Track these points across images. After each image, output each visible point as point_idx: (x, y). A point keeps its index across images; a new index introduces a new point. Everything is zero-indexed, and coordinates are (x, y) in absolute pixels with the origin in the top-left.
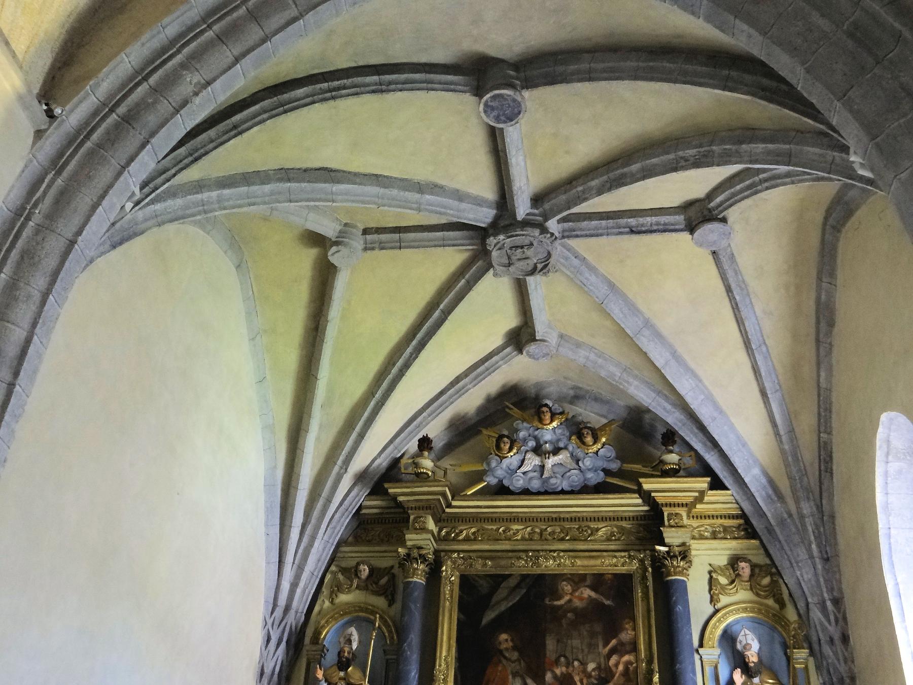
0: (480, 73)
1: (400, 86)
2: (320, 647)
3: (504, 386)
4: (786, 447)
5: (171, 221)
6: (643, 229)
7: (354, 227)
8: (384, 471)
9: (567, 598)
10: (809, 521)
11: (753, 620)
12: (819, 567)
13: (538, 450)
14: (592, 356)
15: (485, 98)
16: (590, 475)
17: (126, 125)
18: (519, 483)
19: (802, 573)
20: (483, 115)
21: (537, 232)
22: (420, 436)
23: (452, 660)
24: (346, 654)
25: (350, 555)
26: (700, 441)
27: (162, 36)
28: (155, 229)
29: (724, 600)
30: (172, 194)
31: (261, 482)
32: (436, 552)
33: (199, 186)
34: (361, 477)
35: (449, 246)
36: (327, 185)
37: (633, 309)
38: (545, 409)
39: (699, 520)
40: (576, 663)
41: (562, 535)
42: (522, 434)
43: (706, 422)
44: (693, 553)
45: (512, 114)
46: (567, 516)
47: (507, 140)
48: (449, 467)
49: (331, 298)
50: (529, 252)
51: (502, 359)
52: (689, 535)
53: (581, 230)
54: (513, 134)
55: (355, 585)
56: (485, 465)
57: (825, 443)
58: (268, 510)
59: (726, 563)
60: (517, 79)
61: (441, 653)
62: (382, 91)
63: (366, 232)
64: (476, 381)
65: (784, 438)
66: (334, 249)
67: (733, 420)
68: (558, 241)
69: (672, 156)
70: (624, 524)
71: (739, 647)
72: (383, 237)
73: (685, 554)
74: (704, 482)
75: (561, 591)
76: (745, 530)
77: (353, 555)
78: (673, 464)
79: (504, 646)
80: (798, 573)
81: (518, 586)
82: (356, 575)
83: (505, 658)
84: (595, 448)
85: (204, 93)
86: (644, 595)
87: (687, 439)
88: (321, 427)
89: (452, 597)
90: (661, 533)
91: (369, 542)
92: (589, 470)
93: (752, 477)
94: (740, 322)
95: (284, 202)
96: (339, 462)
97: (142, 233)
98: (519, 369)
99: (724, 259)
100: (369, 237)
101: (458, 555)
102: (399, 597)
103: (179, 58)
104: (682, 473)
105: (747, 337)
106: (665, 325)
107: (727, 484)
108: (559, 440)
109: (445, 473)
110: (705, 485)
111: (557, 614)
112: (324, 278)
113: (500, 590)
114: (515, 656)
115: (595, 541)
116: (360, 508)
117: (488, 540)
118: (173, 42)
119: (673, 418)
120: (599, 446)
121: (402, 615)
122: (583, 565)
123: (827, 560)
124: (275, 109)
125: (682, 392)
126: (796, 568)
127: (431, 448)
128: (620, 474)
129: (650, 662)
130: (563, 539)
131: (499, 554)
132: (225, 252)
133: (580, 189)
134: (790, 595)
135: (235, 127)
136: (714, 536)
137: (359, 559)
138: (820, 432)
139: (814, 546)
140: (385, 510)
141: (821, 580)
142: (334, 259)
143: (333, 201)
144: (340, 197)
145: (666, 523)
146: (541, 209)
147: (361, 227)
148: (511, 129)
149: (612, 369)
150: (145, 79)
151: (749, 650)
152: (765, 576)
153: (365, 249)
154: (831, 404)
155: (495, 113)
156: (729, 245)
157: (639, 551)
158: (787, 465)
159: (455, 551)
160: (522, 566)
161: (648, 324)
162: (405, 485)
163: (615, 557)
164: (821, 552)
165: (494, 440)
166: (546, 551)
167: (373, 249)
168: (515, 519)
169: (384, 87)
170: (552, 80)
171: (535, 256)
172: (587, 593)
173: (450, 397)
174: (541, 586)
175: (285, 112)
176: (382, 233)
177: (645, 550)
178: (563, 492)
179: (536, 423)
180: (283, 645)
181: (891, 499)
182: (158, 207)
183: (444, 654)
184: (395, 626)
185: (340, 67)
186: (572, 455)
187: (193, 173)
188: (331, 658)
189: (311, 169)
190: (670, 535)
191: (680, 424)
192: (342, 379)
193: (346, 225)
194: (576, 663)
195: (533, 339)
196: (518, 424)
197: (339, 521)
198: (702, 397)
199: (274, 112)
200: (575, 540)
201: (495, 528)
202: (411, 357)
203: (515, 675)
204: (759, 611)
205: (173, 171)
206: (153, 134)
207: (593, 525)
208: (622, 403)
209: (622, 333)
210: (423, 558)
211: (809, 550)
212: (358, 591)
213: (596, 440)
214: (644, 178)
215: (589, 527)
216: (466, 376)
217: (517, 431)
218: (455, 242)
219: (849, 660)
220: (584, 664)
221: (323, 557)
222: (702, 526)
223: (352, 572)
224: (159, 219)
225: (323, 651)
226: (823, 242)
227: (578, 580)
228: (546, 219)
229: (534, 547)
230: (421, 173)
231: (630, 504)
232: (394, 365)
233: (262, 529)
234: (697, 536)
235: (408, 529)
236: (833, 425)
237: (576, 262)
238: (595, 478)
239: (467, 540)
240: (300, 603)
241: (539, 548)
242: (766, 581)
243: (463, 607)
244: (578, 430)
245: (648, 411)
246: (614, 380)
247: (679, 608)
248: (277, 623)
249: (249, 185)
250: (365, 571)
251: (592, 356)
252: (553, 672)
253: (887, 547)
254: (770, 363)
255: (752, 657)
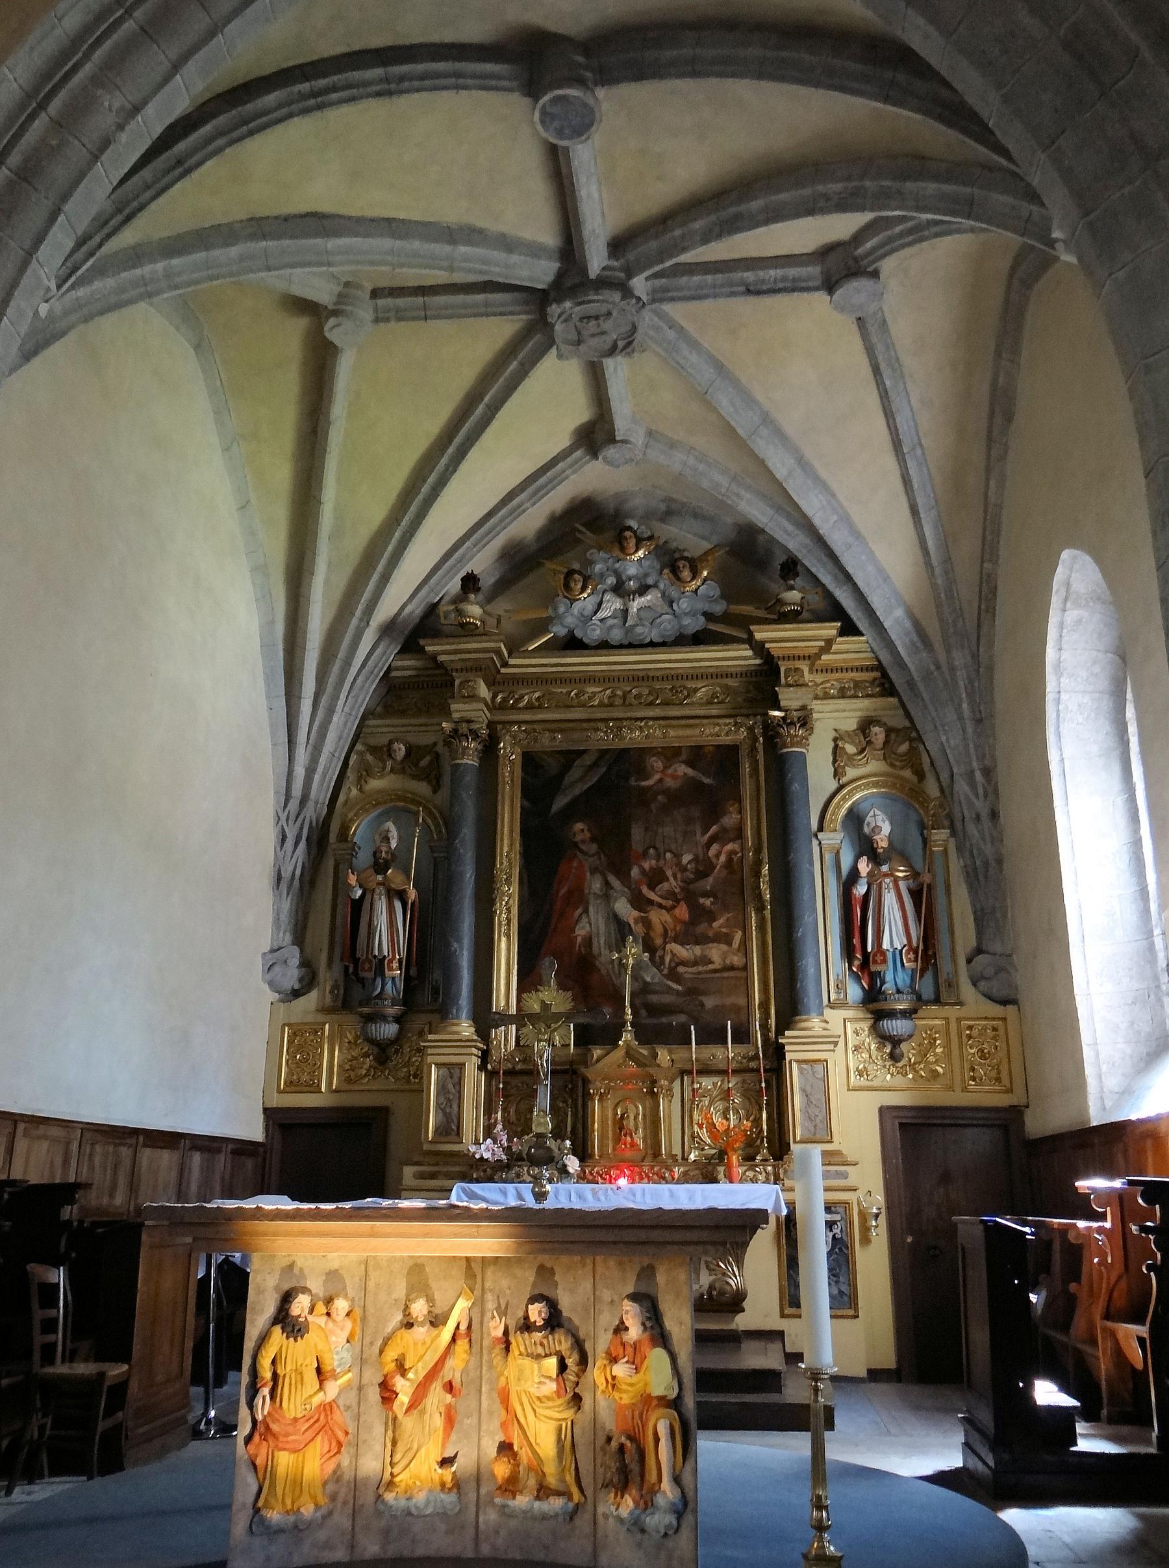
0: (534, 61)
1: (416, 84)
2: (350, 845)
3: (573, 499)
4: (939, 582)
5: (102, 312)
6: (764, 288)
7: (359, 287)
8: (417, 620)
9: (657, 777)
10: (961, 675)
11: (883, 796)
12: (970, 730)
13: (619, 589)
14: (691, 461)
15: (542, 102)
16: (687, 621)
17: (25, 185)
18: (594, 634)
19: (947, 738)
20: (539, 127)
21: (616, 296)
22: (463, 573)
23: (516, 857)
24: (383, 855)
25: (380, 730)
26: (829, 573)
27: (58, 32)
28: (82, 327)
29: (851, 773)
30: (100, 271)
31: (257, 643)
32: (491, 725)
33: (137, 256)
34: (388, 629)
35: (495, 314)
36: (318, 241)
37: (749, 400)
38: (628, 534)
39: (824, 674)
40: (668, 855)
41: (651, 698)
42: (598, 568)
43: (838, 549)
44: (815, 716)
45: (582, 126)
46: (658, 674)
47: (575, 163)
48: (501, 613)
49: (331, 390)
50: (607, 325)
51: (571, 466)
52: (811, 696)
53: (680, 289)
54: (584, 156)
55: (389, 768)
56: (550, 610)
57: (989, 575)
58: (269, 677)
59: (855, 727)
60: (586, 68)
61: (502, 850)
62: (390, 93)
63: (375, 293)
64: (533, 500)
65: (938, 571)
66: (332, 321)
67: (874, 547)
68: (648, 307)
69: (807, 192)
70: (732, 682)
71: (866, 830)
72: (401, 302)
73: (805, 720)
74: (832, 628)
75: (649, 767)
76: (882, 685)
77: (385, 730)
78: (794, 604)
79: (578, 838)
80: (944, 738)
81: (595, 764)
82: (390, 755)
83: (582, 851)
84: (693, 585)
85: (132, 126)
86: (750, 771)
87: (813, 570)
88: (329, 565)
89: (512, 781)
90: (776, 694)
91: (402, 713)
92: (686, 614)
93: (894, 619)
94: (889, 415)
95: (260, 270)
96: (358, 613)
97: (64, 333)
98: (592, 477)
99: (872, 329)
100: (381, 302)
101: (519, 727)
102: (446, 779)
103: (88, 68)
104: (805, 615)
105: (898, 435)
106: (791, 421)
107: (861, 628)
108: (646, 575)
109: (499, 621)
110: (834, 632)
111: (644, 798)
112: (320, 362)
113: (573, 769)
114: (594, 847)
115: (693, 704)
116: (389, 669)
117: (557, 706)
118: (76, 41)
119: (795, 542)
120: (699, 582)
121: (452, 805)
122: (676, 736)
123: (980, 721)
124: (235, 129)
125: (809, 512)
126: (941, 733)
127: (479, 589)
128: (726, 618)
129: (758, 850)
130: (651, 704)
131: (571, 725)
132: (177, 329)
133: (678, 232)
134: (932, 763)
135: (179, 162)
136: (842, 694)
137: (390, 736)
138: (983, 562)
139: (965, 706)
140: (423, 667)
141: (971, 746)
142: (333, 336)
143: (329, 264)
144: (338, 258)
145: (783, 681)
146: (622, 261)
147: (369, 286)
148: (580, 146)
149: (718, 477)
150: (42, 106)
151: (879, 833)
152: (900, 742)
153: (377, 320)
154: (1000, 523)
155: (556, 124)
156: (881, 308)
157: (747, 716)
158: (939, 605)
159: (513, 723)
160: (601, 739)
161: (767, 419)
162: (446, 640)
163: (718, 724)
164: (973, 712)
165: (562, 577)
166: (631, 719)
167: (388, 320)
168: (591, 679)
169: (393, 86)
170: (640, 73)
171: (613, 330)
172: (682, 769)
173: (501, 521)
174: (625, 763)
175: (251, 133)
176: (398, 296)
177: (755, 715)
178: (652, 644)
179: (617, 552)
180: (303, 844)
181: (1065, 655)
182: (81, 292)
183: (506, 849)
184: (443, 818)
185: (326, 55)
186: (663, 594)
187: (128, 237)
188: (364, 858)
189: (295, 216)
190: (787, 697)
191: (804, 551)
192: (354, 502)
193: (347, 284)
194: (668, 855)
195: (611, 440)
196: (593, 554)
197: (361, 688)
198: (835, 518)
199: (235, 135)
200: (667, 704)
201: (564, 691)
202: (447, 469)
203: (594, 871)
204: (894, 786)
205: (97, 239)
206: (65, 197)
207: (691, 684)
208: (729, 520)
209: (730, 432)
210: (475, 735)
211: (958, 710)
212: (392, 775)
213: (695, 574)
214: (767, 222)
215: (685, 688)
216: (522, 491)
217: (591, 563)
218: (502, 309)
219: (997, 840)
220: (677, 856)
221: (345, 735)
222: (828, 681)
223: (383, 752)
224: (85, 311)
225: (354, 849)
226: (1007, 301)
227: (671, 754)
228: (630, 274)
229: (615, 715)
230: (451, 213)
231: (738, 656)
232: (424, 481)
233: (262, 703)
234: (821, 694)
235: (453, 697)
236: (1001, 553)
237: (671, 335)
238: (693, 624)
239: (530, 707)
240: (320, 792)
241: (621, 715)
242: (904, 748)
243: (527, 791)
244: (672, 562)
245: (763, 531)
246: (720, 493)
247: (796, 787)
248: (292, 818)
249: (207, 249)
250: (400, 750)
251: (691, 461)
252: (641, 867)
253: (1054, 715)
254: (925, 470)
255: (882, 841)
